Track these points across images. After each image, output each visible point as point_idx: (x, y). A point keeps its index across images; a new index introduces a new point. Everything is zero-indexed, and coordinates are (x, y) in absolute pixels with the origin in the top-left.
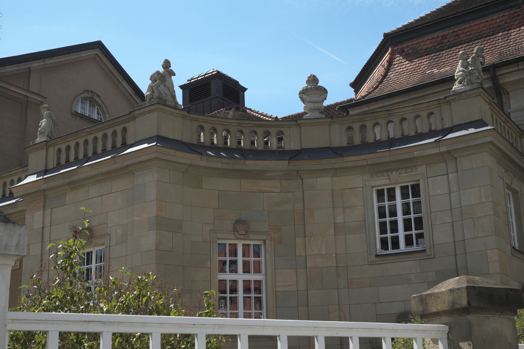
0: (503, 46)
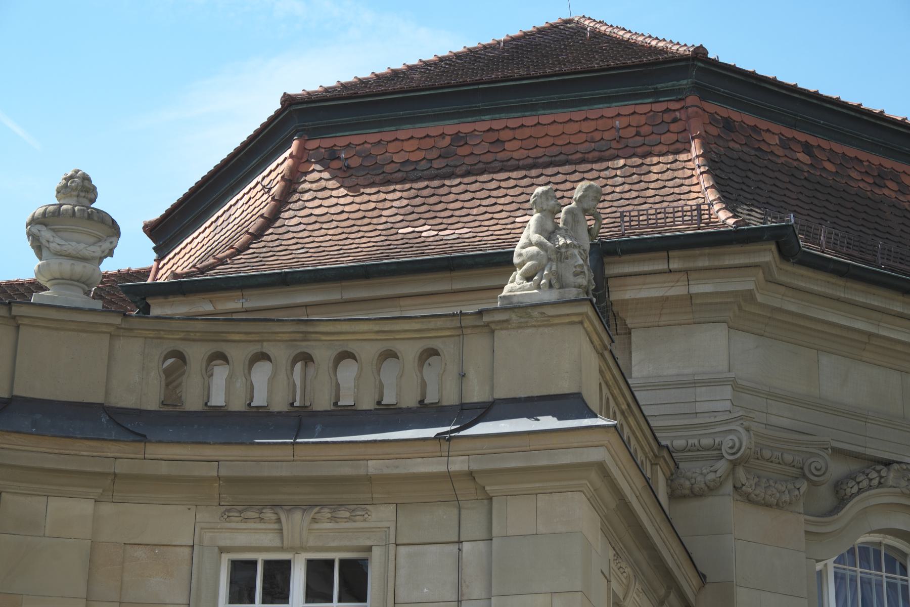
0: (627, 196)
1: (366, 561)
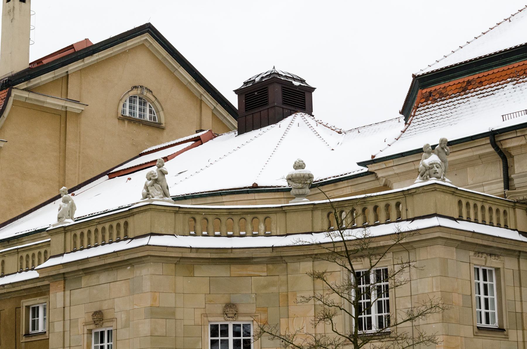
1: (249, 326)
